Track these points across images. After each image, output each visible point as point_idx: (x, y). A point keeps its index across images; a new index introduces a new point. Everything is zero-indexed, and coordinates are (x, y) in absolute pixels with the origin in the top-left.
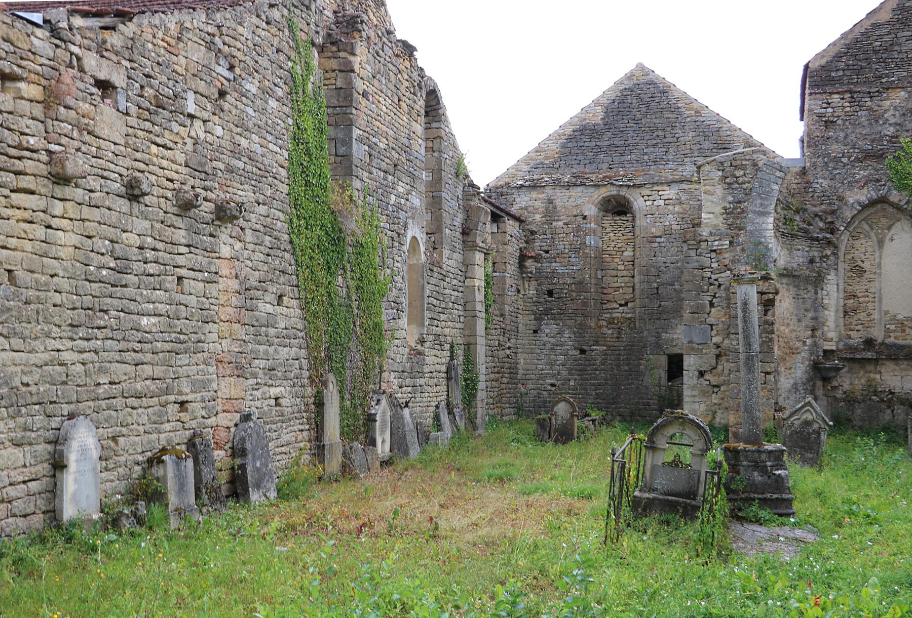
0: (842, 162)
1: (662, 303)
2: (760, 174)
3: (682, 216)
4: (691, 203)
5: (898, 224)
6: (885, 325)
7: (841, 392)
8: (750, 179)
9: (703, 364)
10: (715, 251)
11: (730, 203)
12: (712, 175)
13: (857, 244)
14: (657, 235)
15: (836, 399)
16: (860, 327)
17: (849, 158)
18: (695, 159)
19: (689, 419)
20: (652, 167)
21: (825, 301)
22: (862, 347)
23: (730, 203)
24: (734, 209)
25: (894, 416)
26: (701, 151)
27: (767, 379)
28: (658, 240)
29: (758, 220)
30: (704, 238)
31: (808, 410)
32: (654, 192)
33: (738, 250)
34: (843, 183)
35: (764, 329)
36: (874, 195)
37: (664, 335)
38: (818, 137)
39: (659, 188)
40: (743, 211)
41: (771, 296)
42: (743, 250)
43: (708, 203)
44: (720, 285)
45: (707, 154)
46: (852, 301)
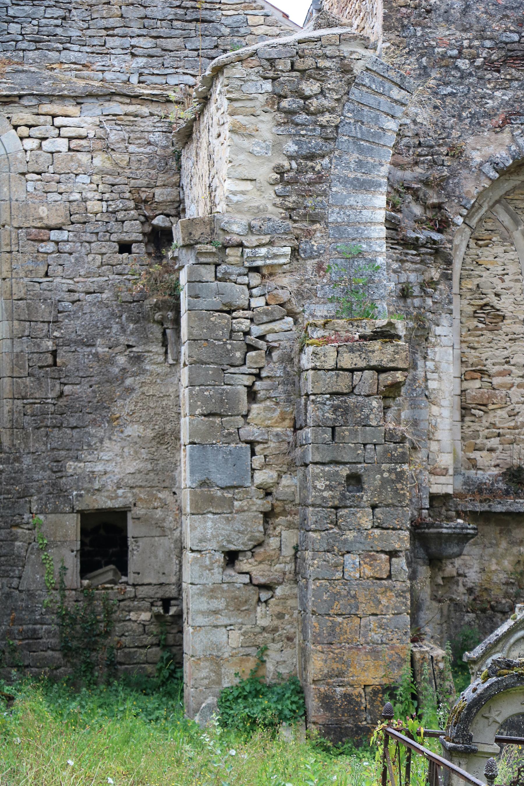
0: (457, 68)
1: (66, 388)
2: (356, 93)
3: (110, 179)
4: (132, 148)
7: (461, 589)
8: (334, 104)
9: (234, 536)
10: (256, 269)
11: (291, 158)
12: (250, 88)
14: (53, 222)
15: (457, 606)
16: (494, 442)
17: (473, 59)
18: (134, 41)
20: (30, 54)
21: (432, 385)
22: (503, 487)
23: (291, 158)
24: (298, 172)
26: (147, 22)
28: (54, 235)
29: (352, 201)
30: (236, 239)
32: (42, 119)
33: (309, 268)
34: (460, 116)
35: (386, 451)
37: (71, 466)
39: (54, 108)
40: (320, 179)
41: (399, 376)
42: (320, 267)
43: (242, 157)
44: (270, 350)
45: (163, 32)
46: (477, 384)
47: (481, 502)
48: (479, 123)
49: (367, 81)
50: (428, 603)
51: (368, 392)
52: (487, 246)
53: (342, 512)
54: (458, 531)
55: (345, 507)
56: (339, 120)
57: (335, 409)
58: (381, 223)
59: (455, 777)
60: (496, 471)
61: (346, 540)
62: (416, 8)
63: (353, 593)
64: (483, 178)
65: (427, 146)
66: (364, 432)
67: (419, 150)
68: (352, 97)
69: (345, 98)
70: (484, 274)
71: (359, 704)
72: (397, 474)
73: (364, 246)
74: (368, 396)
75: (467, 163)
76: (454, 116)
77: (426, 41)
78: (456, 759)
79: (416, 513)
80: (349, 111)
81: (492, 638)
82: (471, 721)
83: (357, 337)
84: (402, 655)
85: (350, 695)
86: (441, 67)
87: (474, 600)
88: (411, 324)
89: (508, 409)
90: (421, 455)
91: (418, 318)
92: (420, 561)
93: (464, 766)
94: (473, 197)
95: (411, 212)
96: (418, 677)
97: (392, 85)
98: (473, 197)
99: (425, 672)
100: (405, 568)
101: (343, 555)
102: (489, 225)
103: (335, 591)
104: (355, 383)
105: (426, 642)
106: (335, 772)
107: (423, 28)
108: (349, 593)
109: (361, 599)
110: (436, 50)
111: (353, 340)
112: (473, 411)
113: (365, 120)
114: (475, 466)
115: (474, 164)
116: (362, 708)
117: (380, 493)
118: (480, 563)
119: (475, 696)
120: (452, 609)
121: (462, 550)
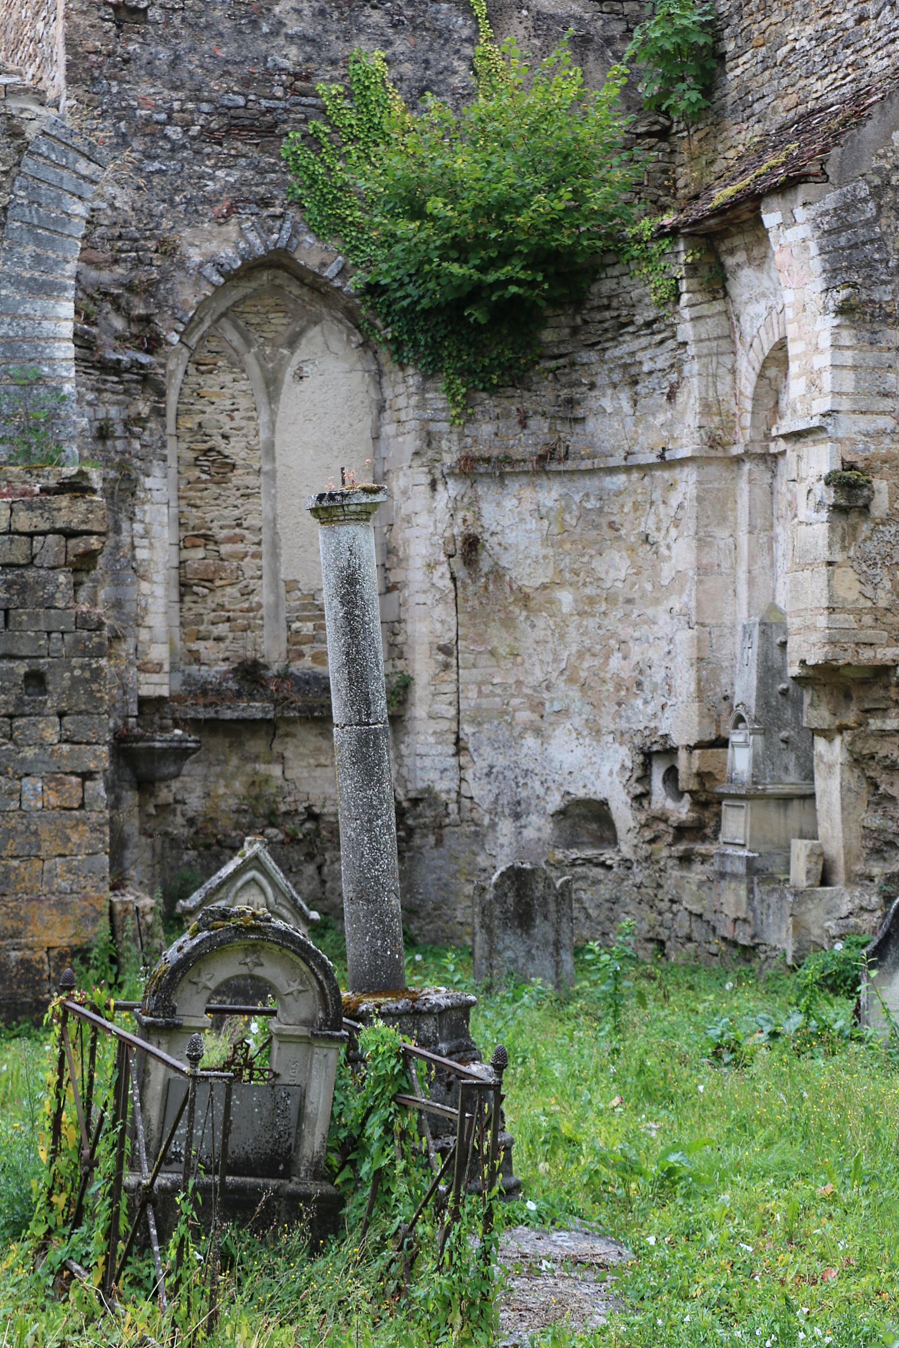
0: (166, 137)
5: (314, 332)
6: (289, 623)
7: (180, 820)
13: (211, 383)
15: (174, 842)
16: (222, 629)
17: (186, 126)
19: (277, 931)
21: (141, 554)
25: (323, 882)
27: (89, 792)
29: (27, 308)
31: (253, 880)
34: (172, 201)
35: (78, 641)
36: (257, 244)
38: (97, 52)
41: (94, 542)
46: (200, 553)
47: (205, 706)
48: (196, 211)
49: (44, 148)
50: (136, 839)
51: (52, 564)
52: (210, 372)
53: (19, 722)
54: (175, 744)
55: (23, 715)
56: (7, 199)
57: (9, 585)
58: (68, 339)
59: (152, 1061)
60: (224, 667)
61: (24, 759)
62: (109, 56)
63: (33, 828)
64: (204, 283)
65: (130, 239)
66: (48, 616)
67: (120, 244)
68: (25, 170)
69: (15, 170)
70: (208, 409)
71: (40, 972)
72: (92, 671)
73: (46, 369)
74: (53, 568)
75: (183, 263)
76: (164, 201)
77: (124, 99)
78: (154, 1038)
79: (120, 722)
80: (20, 188)
81: (215, 880)
82: (174, 989)
83: (37, 489)
84: (98, 907)
85: (29, 961)
86: (145, 135)
87: (196, 833)
88: (112, 474)
89: (240, 586)
90: (126, 647)
91: (122, 466)
92: (126, 785)
93: (165, 1046)
94: (191, 308)
95: (110, 325)
96: (119, 936)
97: (77, 156)
98: (191, 308)
99: (128, 927)
100: (103, 794)
101: (20, 779)
102: (213, 346)
103: (9, 826)
104: (35, 551)
105: (130, 889)
106: (6, 1061)
107: (120, 82)
108: (27, 828)
109: (44, 835)
110: (138, 112)
111: (31, 493)
112: (195, 589)
113: (43, 200)
114: (198, 661)
115: (192, 265)
116: (45, 976)
117: (70, 696)
118: (204, 786)
119: (181, 956)
120: (167, 845)
121: (180, 769)
